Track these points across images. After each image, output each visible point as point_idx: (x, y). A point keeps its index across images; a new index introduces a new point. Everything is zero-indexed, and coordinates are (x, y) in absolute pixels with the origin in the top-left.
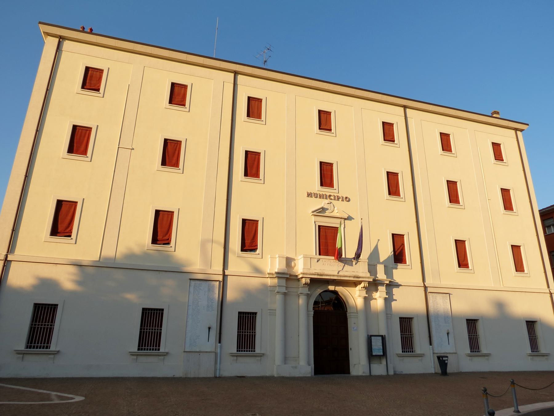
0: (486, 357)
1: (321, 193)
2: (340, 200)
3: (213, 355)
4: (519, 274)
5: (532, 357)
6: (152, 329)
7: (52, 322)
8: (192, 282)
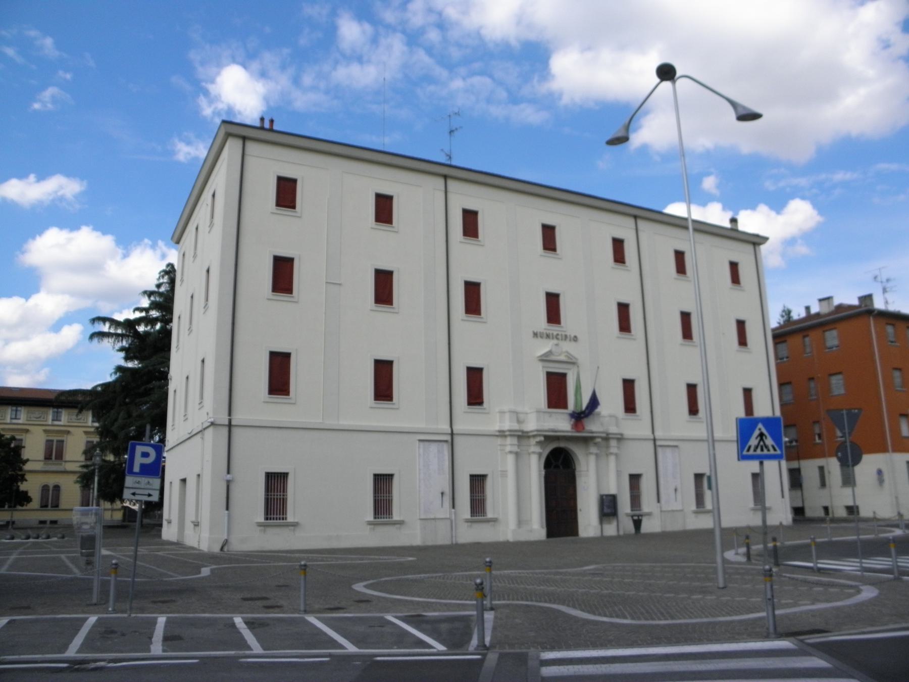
1: (548, 332)
2: (568, 339)
3: (448, 522)
7: (284, 492)
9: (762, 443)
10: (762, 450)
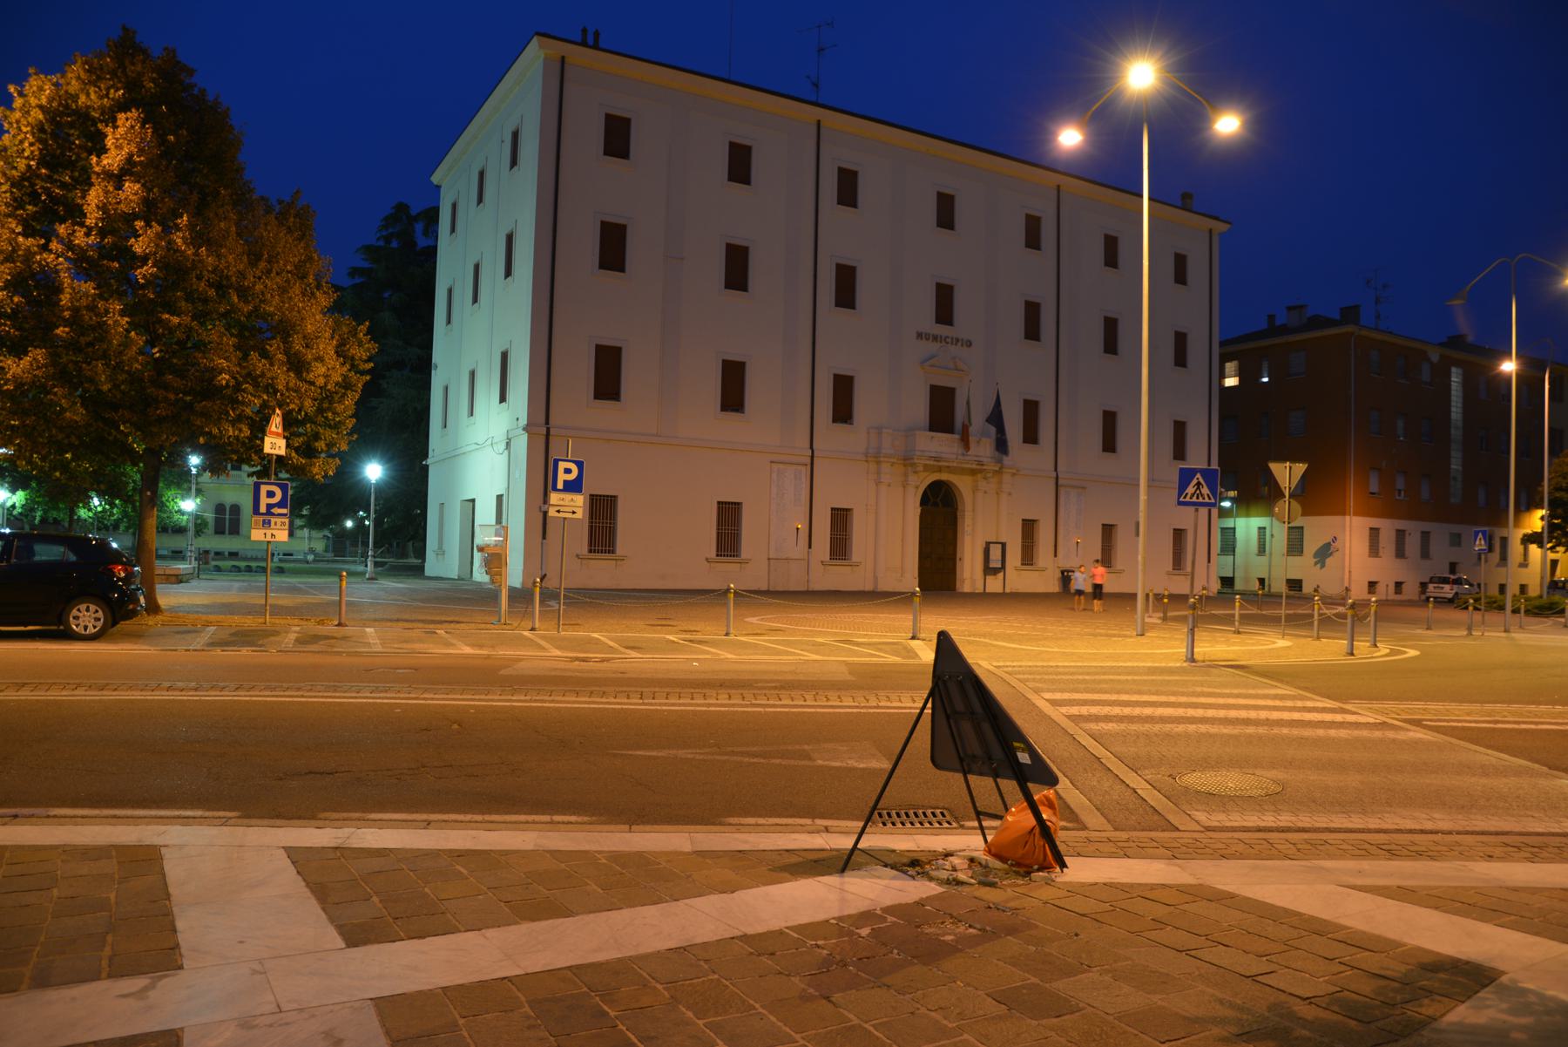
0: (1118, 574)
2: (960, 344)
6: (607, 523)
8: (774, 465)
9: (1198, 492)
10: (1198, 498)
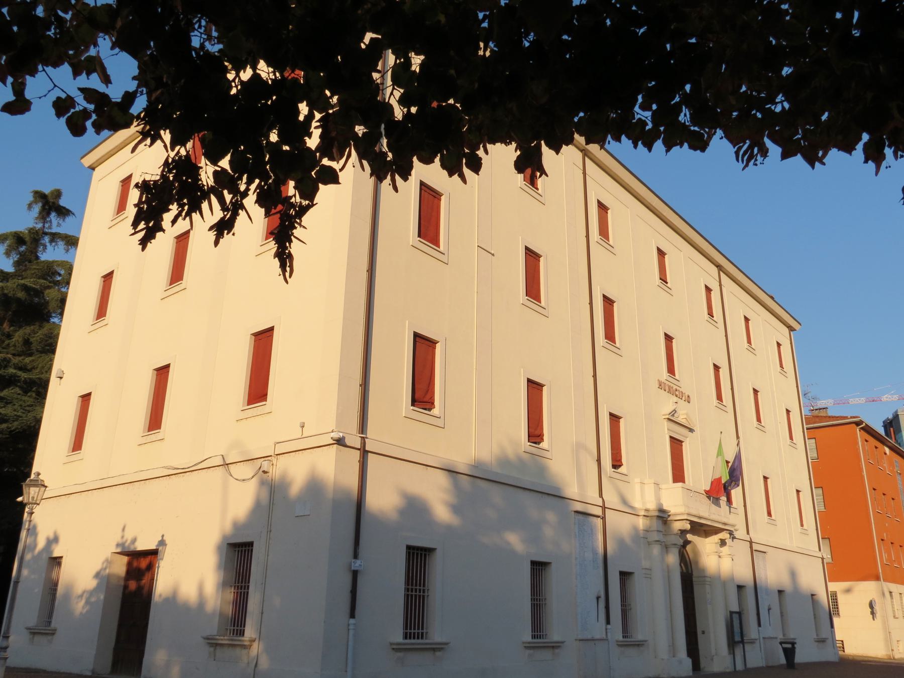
4: (418, 414)
5: (531, 651)
